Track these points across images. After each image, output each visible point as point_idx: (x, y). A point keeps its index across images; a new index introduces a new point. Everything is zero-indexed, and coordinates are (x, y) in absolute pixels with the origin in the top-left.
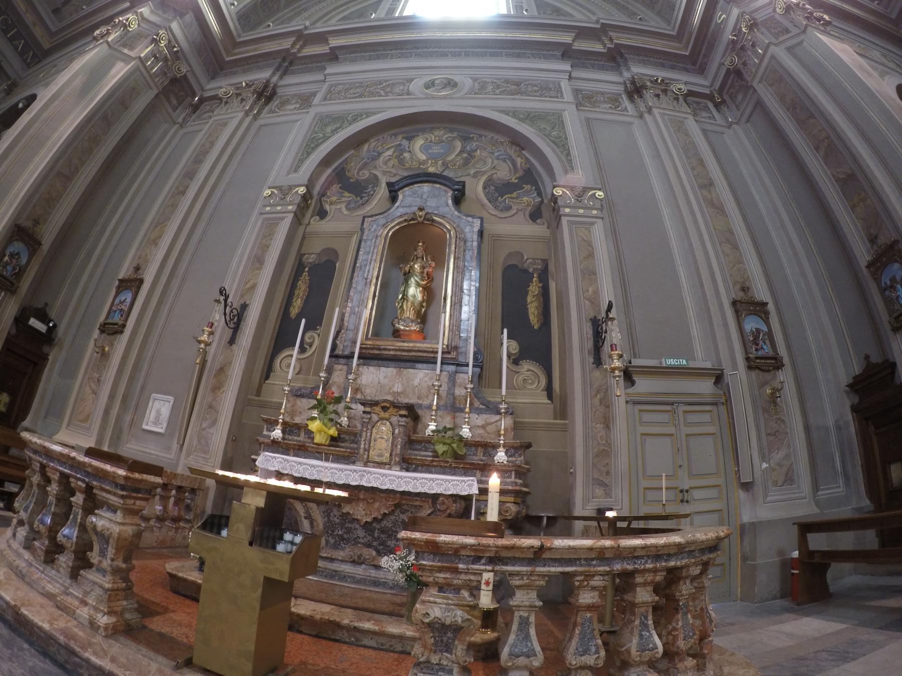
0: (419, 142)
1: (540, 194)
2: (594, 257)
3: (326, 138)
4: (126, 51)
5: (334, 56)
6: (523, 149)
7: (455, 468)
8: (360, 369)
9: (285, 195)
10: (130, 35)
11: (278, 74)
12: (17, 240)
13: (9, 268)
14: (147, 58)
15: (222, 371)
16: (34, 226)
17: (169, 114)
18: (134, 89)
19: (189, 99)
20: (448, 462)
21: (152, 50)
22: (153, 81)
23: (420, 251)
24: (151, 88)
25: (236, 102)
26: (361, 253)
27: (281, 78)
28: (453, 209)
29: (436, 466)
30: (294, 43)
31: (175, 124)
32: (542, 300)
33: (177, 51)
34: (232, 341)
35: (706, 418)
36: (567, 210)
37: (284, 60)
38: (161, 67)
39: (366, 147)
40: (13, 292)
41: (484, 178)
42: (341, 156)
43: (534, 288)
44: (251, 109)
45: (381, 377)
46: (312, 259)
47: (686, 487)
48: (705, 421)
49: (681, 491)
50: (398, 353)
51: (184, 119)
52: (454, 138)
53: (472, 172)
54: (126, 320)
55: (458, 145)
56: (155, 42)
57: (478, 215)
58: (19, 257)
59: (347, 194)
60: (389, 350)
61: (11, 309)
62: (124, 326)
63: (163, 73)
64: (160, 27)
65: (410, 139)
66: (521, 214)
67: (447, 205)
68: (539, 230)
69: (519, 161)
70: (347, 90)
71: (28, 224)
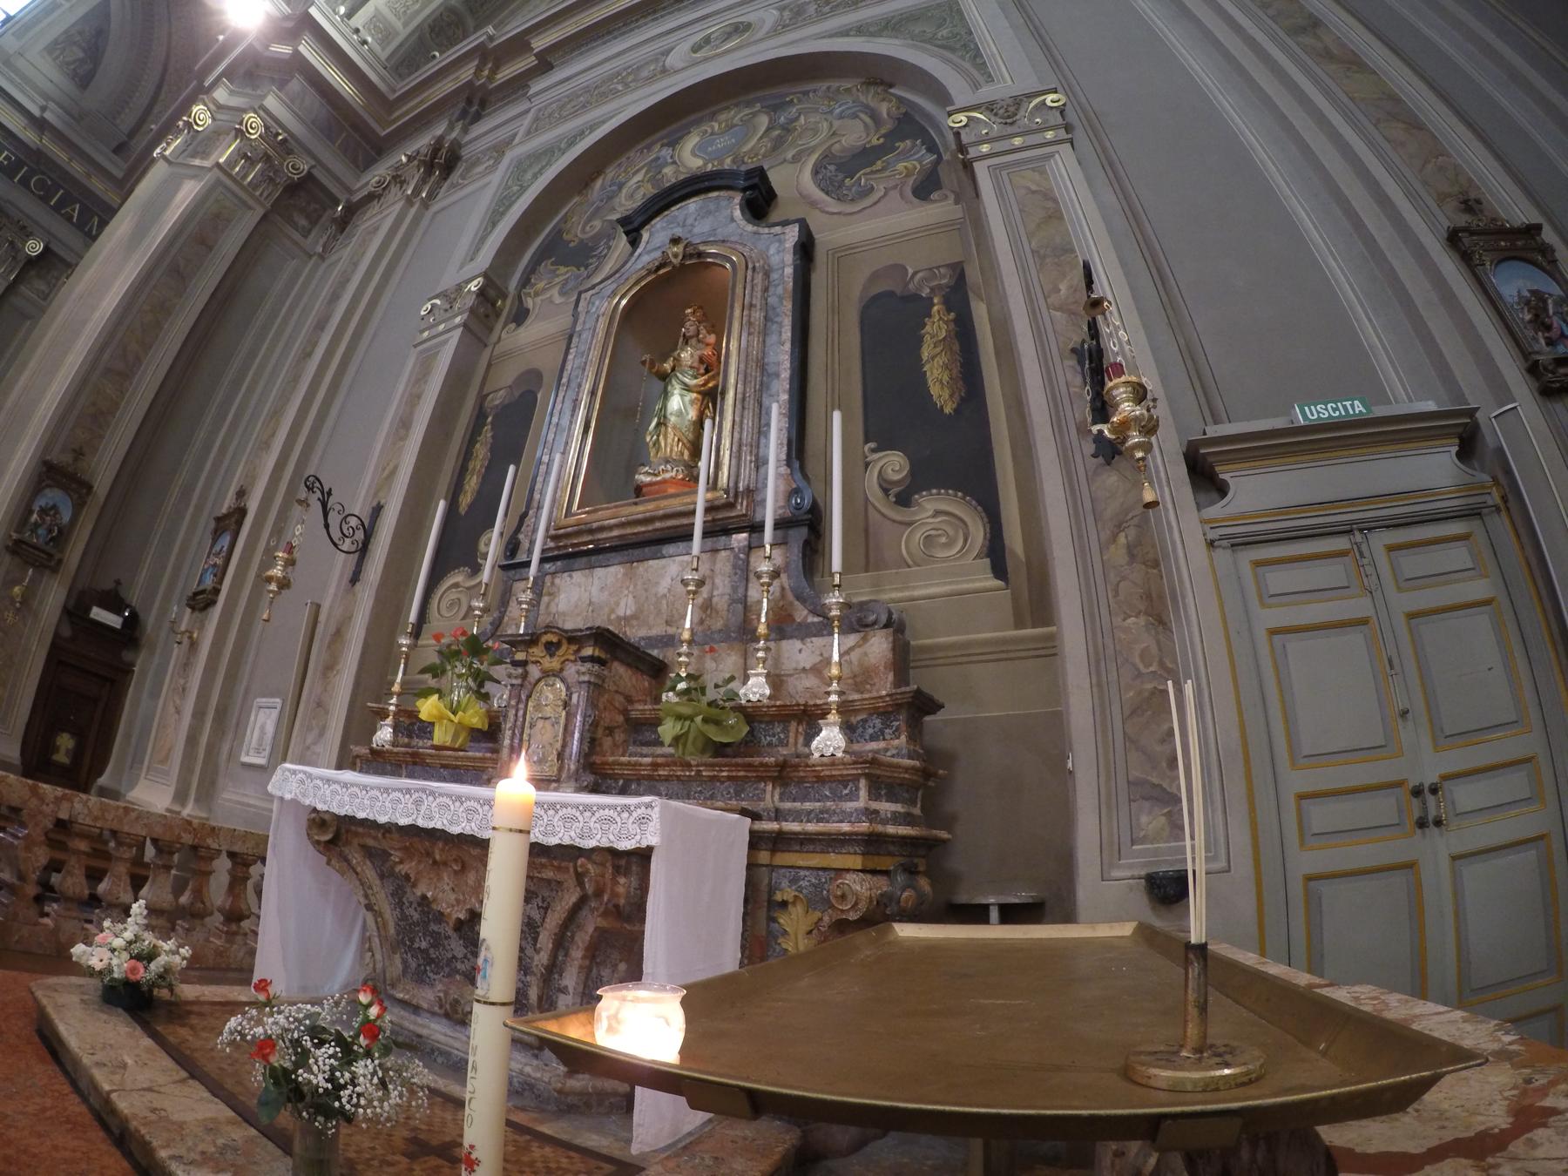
0: (692, 141)
1: (932, 148)
2: (1061, 218)
3: (523, 189)
4: (197, 162)
5: (545, 64)
6: (891, 86)
7: (713, 779)
8: (557, 581)
9: (451, 303)
10: (200, 137)
11: (459, 125)
12: (48, 486)
13: (41, 531)
14: (231, 162)
15: (338, 635)
16: (76, 460)
17: (296, 243)
18: (217, 216)
19: (329, 212)
20: (688, 766)
21: (238, 149)
22: (252, 196)
23: (689, 328)
24: (250, 208)
25: (394, 189)
26: (570, 357)
27: (465, 131)
28: (743, 223)
29: (667, 779)
30: (479, 69)
31: (310, 257)
32: (956, 347)
33: (284, 141)
34: (355, 579)
35: (1458, 557)
36: (985, 148)
37: (469, 102)
38: (262, 172)
39: (599, 183)
40: (55, 570)
41: (815, 157)
42: (556, 213)
43: (937, 327)
44: (417, 192)
45: (595, 590)
46: (497, 399)
47: (1430, 778)
48: (1457, 568)
49: (1417, 792)
50: (629, 531)
51: (324, 247)
52: (754, 115)
53: (789, 155)
54: (221, 582)
55: (763, 121)
56: (240, 133)
57: (794, 218)
58: (57, 512)
59: (562, 269)
60: (610, 528)
61: (53, 597)
62: (217, 591)
63: (268, 178)
64: (245, 111)
65: (673, 144)
66: (895, 194)
67: (733, 220)
68: (940, 210)
69: (884, 109)
70: (562, 108)
71: (66, 459)
